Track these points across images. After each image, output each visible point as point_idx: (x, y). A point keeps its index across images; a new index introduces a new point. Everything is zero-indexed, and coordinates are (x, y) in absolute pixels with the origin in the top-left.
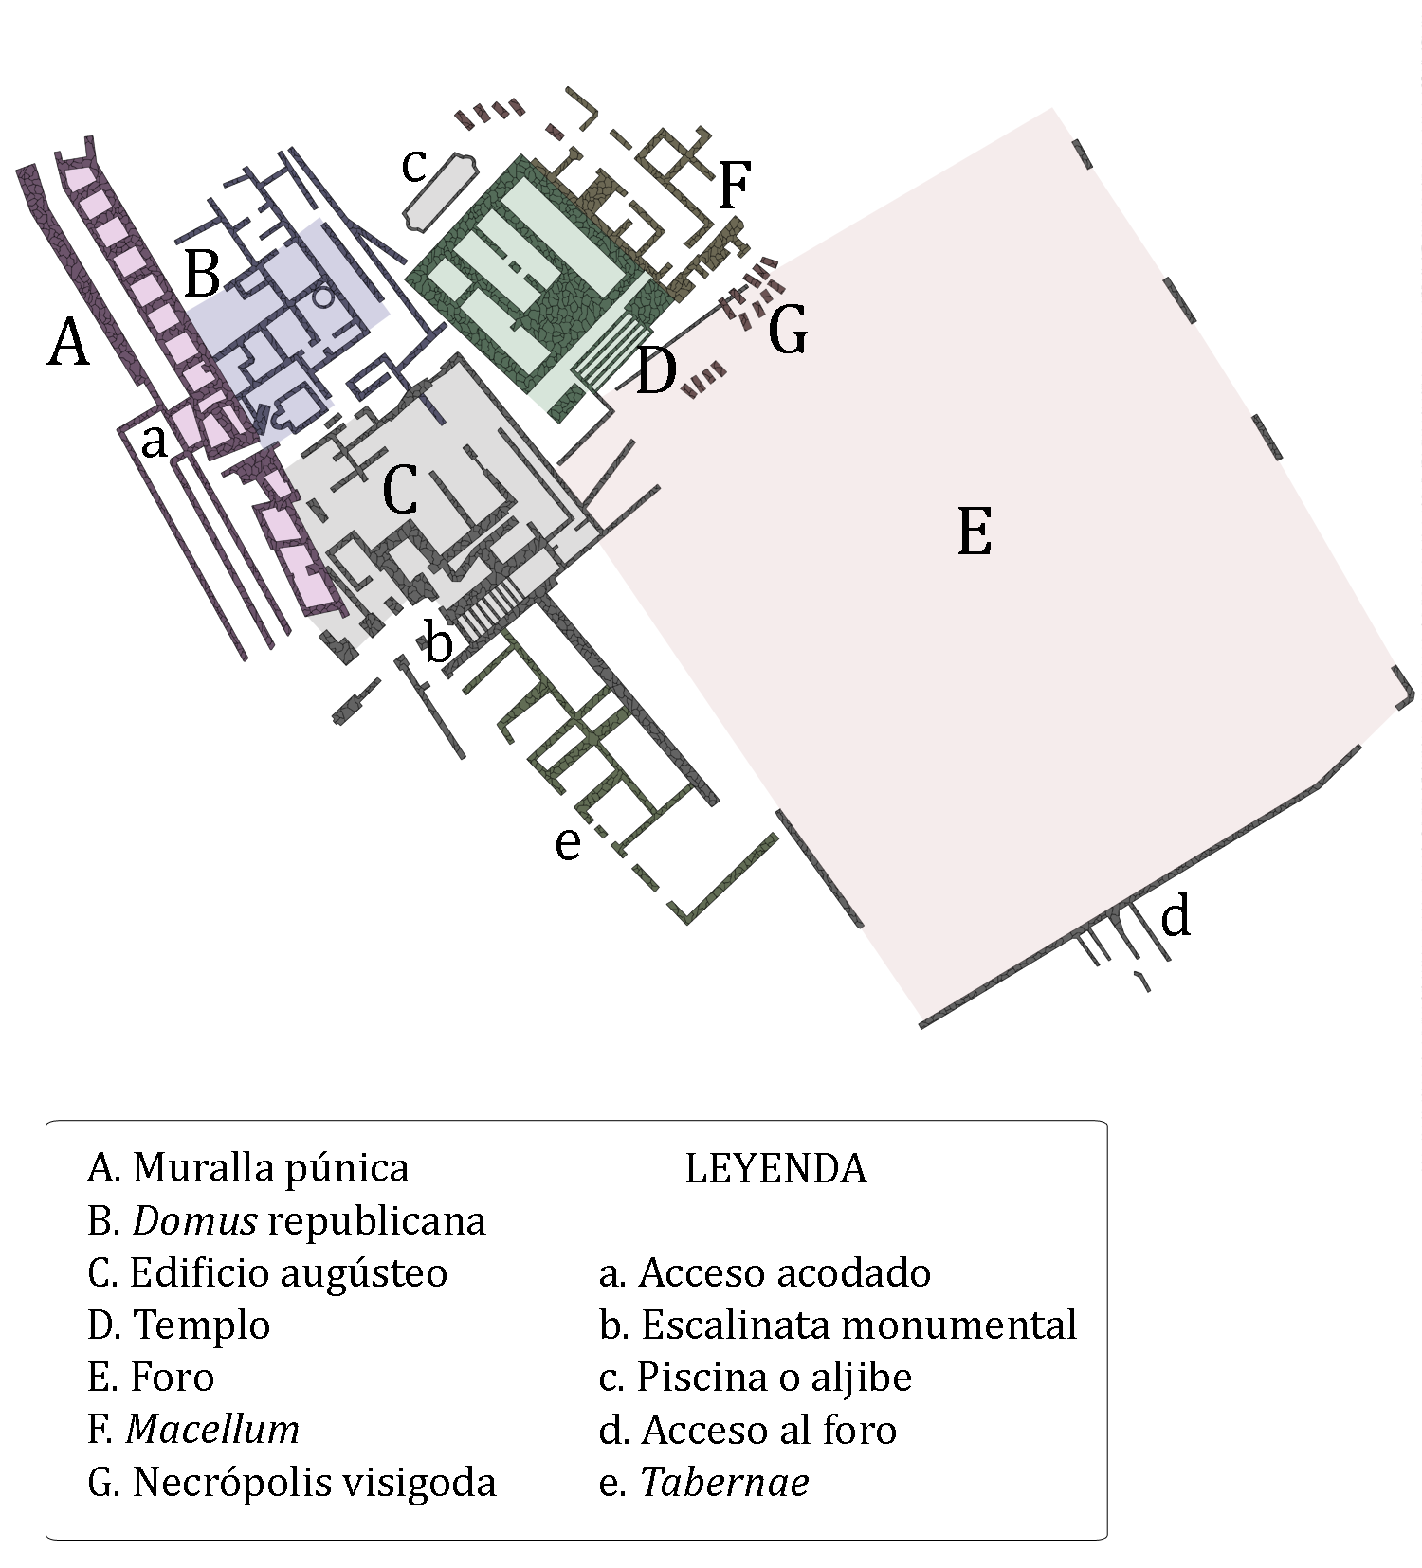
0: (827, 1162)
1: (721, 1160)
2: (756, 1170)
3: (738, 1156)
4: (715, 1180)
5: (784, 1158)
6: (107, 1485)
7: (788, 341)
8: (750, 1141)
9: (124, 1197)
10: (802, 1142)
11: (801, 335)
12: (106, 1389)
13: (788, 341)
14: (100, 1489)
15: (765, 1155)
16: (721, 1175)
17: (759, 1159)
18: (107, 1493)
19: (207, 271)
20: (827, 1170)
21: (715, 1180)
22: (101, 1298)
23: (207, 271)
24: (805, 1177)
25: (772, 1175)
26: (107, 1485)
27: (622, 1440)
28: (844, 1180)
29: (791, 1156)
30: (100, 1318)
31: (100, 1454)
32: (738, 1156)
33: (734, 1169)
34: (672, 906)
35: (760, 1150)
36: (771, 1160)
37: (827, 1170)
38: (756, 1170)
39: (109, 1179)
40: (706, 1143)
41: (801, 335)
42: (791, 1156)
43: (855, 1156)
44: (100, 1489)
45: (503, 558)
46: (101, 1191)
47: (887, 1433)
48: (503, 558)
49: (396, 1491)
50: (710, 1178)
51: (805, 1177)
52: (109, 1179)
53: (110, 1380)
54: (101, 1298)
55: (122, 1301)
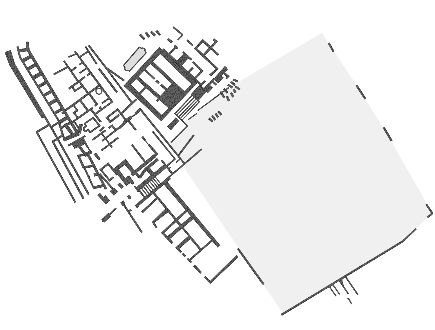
45: (154, 171)
48: (154, 171)
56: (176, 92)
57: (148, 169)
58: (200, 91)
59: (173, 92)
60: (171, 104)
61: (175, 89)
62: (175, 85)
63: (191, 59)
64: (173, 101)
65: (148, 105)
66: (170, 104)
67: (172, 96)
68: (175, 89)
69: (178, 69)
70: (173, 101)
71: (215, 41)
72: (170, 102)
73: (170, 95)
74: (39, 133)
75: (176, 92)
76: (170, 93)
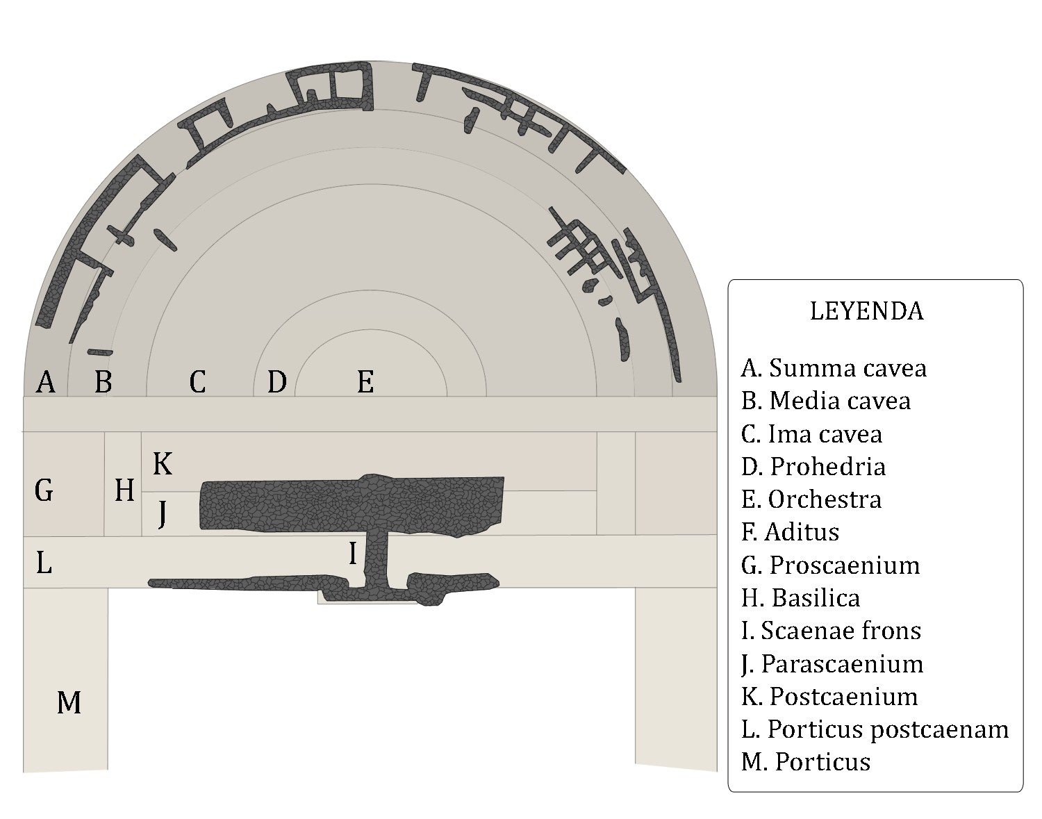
0: (899, 306)
1: (832, 306)
2: (854, 313)
3: (843, 303)
4: (828, 318)
5: (872, 305)
6: (754, 567)
7: (44, 495)
8: (850, 293)
9: (763, 388)
10: (883, 294)
11: (49, 492)
12: (753, 507)
13: (44, 495)
14: (749, 569)
15: (859, 303)
16: (832, 315)
17: (856, 305)
18: (754, 572)
19: (106, 381)
20: (899, 312)
21: (828, 318)
22: (750, 449)
23: (106, 381)
24: (885, 317)
25: (864, 315)
26: (754, 567)
27: (748, 636)
28: (910, 318)
29: (876, 303)
30: (750, 463)
31: (749, 547)
32: (843, 303)
33: (841, 311)
34: (191, 164)
35: (856, 300)
36: (863, 306)
37: (899, 312)
38: (854, 313)
39: (754, 375)
40: (824, 293)
41: (49, 492)
42: (876, 303)
43: (916, 303)
44: (749, 569)
46: (750, 383)
47: (551, 243)
49: (814, 603)
50: (825, 316)
51: (885, 317)
52: (754, 375)
53: (756, 501)
54: (750, 449)
55: (764, 453)
56: (405, 509)
57: (573, 246)
58: (303, 500)
59: (301, 503)
60: (379, 499)
61: (307, 507)
62: (440, 596)
63: (609, 300)
64: (281, 503)
65: (316, 70)
66: (379, 556)
67: (293, 501)
68: (307, 507)
69: (78, 231)
70: (281, 503)
71: (470, 123)
72: (382, 555)
73: (295, 496)
74: (359, 74)
75: (405, 509)
76: (299, 497)
